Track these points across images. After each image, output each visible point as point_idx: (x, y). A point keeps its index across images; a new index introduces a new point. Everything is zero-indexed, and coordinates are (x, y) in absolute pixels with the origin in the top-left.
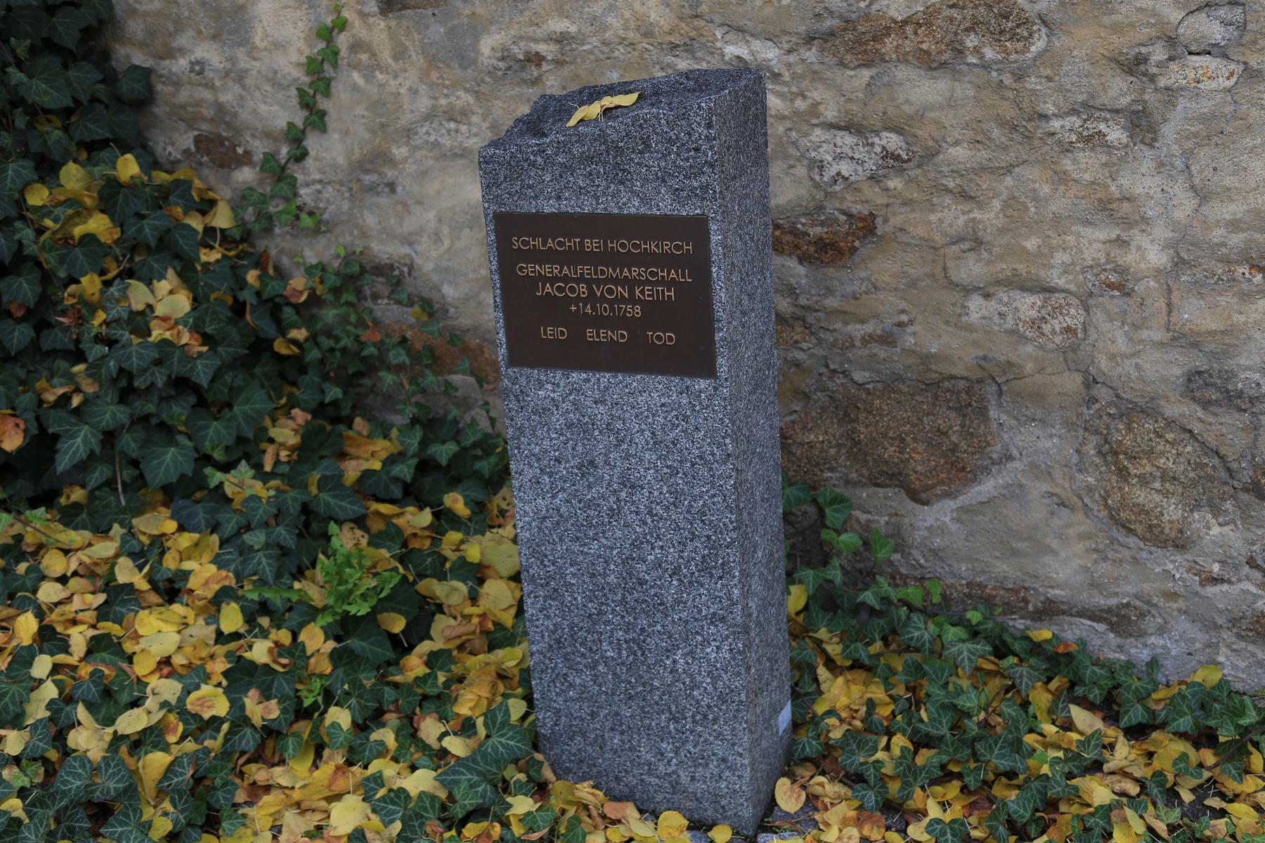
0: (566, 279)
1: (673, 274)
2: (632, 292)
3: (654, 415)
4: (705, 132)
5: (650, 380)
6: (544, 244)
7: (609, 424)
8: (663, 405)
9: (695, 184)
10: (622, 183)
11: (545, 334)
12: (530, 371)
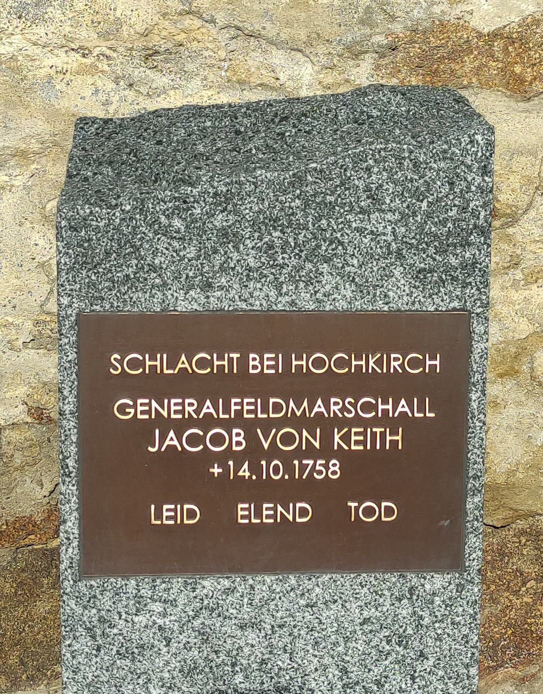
0: (208, 422)
1: (403, 406)
2: (327, 439)
3: (347, 639)
4: (478, 180)
5: (346, 581)
6: (172, 364)
7: (263, 662)
8: (366, 621)
9: (454, 261)
10: (327, 260)
11: (159, 516)
12: (120, 582)
